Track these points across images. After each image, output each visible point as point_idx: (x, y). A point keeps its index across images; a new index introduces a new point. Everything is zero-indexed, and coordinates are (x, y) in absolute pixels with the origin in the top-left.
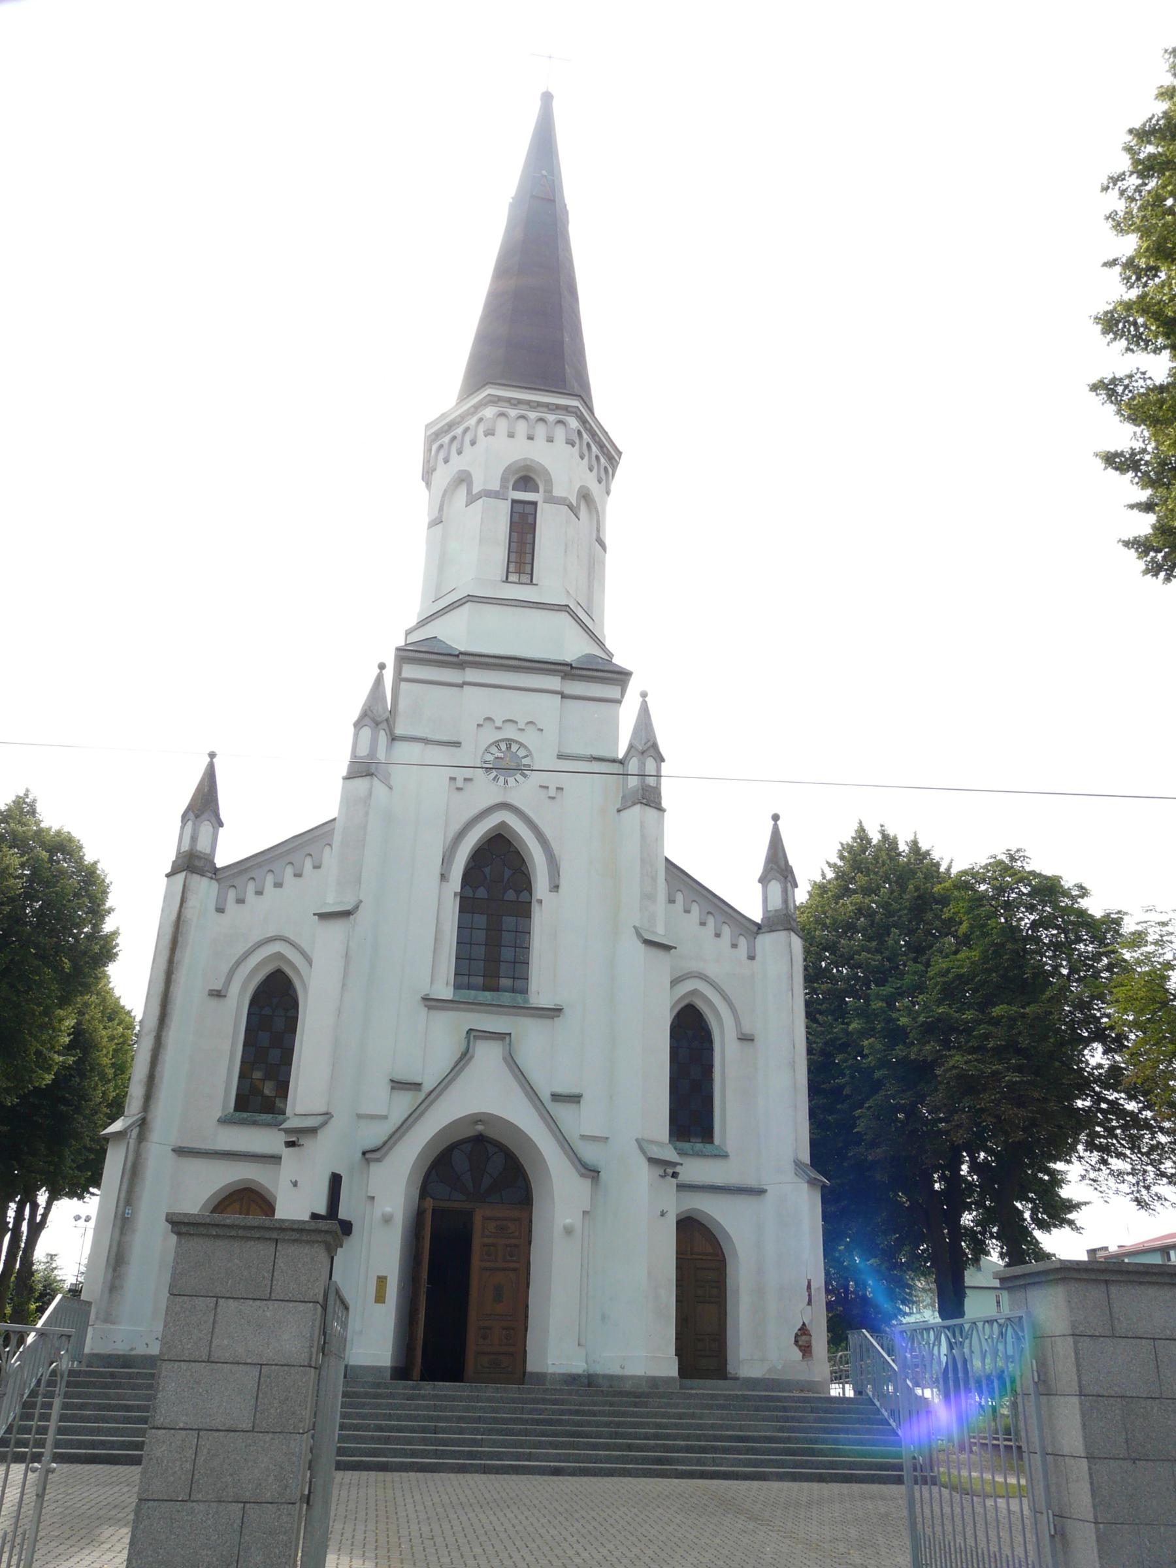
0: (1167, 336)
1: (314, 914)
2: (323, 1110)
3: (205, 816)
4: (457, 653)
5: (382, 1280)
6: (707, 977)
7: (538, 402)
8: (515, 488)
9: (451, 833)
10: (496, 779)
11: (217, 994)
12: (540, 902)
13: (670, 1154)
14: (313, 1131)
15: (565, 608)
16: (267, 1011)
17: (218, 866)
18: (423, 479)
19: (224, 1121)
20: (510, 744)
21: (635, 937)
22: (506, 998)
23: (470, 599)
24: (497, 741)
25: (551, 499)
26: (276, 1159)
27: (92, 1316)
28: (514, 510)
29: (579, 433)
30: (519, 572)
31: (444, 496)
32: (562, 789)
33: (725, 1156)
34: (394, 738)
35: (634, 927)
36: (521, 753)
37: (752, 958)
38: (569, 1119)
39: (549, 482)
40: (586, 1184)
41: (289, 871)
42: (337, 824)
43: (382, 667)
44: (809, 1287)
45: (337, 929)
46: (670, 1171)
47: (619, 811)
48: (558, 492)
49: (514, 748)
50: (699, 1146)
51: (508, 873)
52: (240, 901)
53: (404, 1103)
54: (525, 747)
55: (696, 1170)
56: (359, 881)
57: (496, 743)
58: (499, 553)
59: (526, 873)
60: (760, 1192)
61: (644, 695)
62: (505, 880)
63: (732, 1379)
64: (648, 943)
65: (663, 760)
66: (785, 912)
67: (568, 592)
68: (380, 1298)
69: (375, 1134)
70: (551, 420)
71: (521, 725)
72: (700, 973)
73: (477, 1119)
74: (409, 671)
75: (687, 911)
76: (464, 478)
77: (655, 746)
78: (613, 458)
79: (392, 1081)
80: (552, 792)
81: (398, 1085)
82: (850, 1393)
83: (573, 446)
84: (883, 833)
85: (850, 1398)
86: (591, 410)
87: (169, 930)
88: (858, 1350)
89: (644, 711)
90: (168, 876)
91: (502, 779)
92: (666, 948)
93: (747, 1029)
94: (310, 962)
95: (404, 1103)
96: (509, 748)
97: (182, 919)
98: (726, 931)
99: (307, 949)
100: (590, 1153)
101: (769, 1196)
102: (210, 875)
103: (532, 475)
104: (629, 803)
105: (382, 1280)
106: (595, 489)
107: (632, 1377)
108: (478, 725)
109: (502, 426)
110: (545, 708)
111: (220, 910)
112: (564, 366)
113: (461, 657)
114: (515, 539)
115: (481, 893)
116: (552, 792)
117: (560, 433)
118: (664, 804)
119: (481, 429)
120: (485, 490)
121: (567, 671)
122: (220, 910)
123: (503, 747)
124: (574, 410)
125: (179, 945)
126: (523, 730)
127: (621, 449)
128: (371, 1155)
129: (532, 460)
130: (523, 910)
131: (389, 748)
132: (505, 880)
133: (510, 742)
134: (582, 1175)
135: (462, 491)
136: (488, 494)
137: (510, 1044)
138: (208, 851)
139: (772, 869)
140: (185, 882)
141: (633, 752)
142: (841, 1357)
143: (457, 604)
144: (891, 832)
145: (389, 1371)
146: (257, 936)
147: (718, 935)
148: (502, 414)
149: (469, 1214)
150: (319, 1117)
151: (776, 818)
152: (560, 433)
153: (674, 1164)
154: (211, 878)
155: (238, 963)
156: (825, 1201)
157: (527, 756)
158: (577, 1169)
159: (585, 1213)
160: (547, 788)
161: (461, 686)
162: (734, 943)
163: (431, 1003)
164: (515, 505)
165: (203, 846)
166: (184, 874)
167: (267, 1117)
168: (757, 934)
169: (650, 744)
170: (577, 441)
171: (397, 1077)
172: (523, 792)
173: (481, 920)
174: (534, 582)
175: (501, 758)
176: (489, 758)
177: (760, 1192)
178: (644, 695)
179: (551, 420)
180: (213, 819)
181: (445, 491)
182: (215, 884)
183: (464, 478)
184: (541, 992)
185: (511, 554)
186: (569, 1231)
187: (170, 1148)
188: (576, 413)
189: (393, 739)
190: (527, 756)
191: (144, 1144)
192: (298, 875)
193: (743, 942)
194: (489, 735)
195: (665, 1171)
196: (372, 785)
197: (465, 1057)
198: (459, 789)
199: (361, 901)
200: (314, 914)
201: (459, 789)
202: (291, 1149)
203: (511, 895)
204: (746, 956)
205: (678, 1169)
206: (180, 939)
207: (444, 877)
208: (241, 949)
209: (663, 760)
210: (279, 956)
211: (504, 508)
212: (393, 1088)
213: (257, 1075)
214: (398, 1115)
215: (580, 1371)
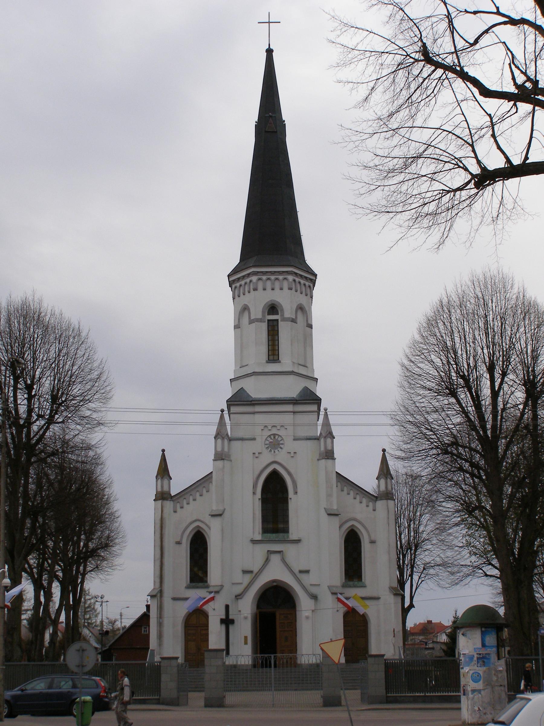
2: (220, 584)
4: (251, 399)
5: (246, 638)
8: (269, 314)
9: (255, 476)
10: (271, 451)
11: (179, 543)
19: (188, 587)
22: (281, 536)
25: (284, 319)
27: (155, 654)
28: (269, 325)
33: (365, 586)
36: (280, 439)
37: (374, 510)
38: (307, 580)
39: (282, 310)
41: (198, 494)
42: (214, 475)
43: (222, 411)
44: (394, 631)
45: (218, 520)
47: (318, 460)
48: (287, 315)
49: (277, 437)
50: (356, 583)
52: (182, 507)
53: (247, 578)
54: (281, 436)
55: (352, 592)
57: (270, 436)
58: (264, 349)
59: (313, 273)
60: (378, 598)
64: (329, 514)
68: (246, 643)
69: (239, 589)
74: (233, 409)
75: (348, 494)
80: (292, 454)
81: (245, 572)
87: (158, 522)
90: (154, 500)
91: (273, 451)
92: (337, 515)
94: (210, 528)
95: (247, 578)
96: (274, 437)
98: (364, 500)
99: (208, 524)
100: (314, 590)
101: (381, 601)
102: (169, 499)
104: (321, 458)
105: (246, 638)
110: (288, 419)
111: (175, 512)
116: (292, 454)
117: (285, 285)
118: (335, 456)
120: (256, 319)
122: (175, 512)
123: (272, 437)
128: (238, 597)
130: (285, 500)
131: (229, 444)
133: (274, 435)
136: (257, 320)
138: (168, 490)
139: (381, 474)
143: (249, 375)
146: (189, 520)
148: (260, 279)
152: (285, 285)
154: (170, 500)
163: (254, 542)
165: (166, 489)
167: (201, 584)
168: (376, 500)
169: (328, 433)
172: (281, 456)
176: (267, 442)
177: (378, 598)
180: (168, 478)
182: (172, 502)
184: (293, 534)
186: (307, 618)
192: (201, 495)
193: (371, 504)
194: (267, 433)
196: (224, 464)
197: (267, 561)
206: (163, 526)
207: (254, 493)
208: (184, 525)
210: (198, 526)
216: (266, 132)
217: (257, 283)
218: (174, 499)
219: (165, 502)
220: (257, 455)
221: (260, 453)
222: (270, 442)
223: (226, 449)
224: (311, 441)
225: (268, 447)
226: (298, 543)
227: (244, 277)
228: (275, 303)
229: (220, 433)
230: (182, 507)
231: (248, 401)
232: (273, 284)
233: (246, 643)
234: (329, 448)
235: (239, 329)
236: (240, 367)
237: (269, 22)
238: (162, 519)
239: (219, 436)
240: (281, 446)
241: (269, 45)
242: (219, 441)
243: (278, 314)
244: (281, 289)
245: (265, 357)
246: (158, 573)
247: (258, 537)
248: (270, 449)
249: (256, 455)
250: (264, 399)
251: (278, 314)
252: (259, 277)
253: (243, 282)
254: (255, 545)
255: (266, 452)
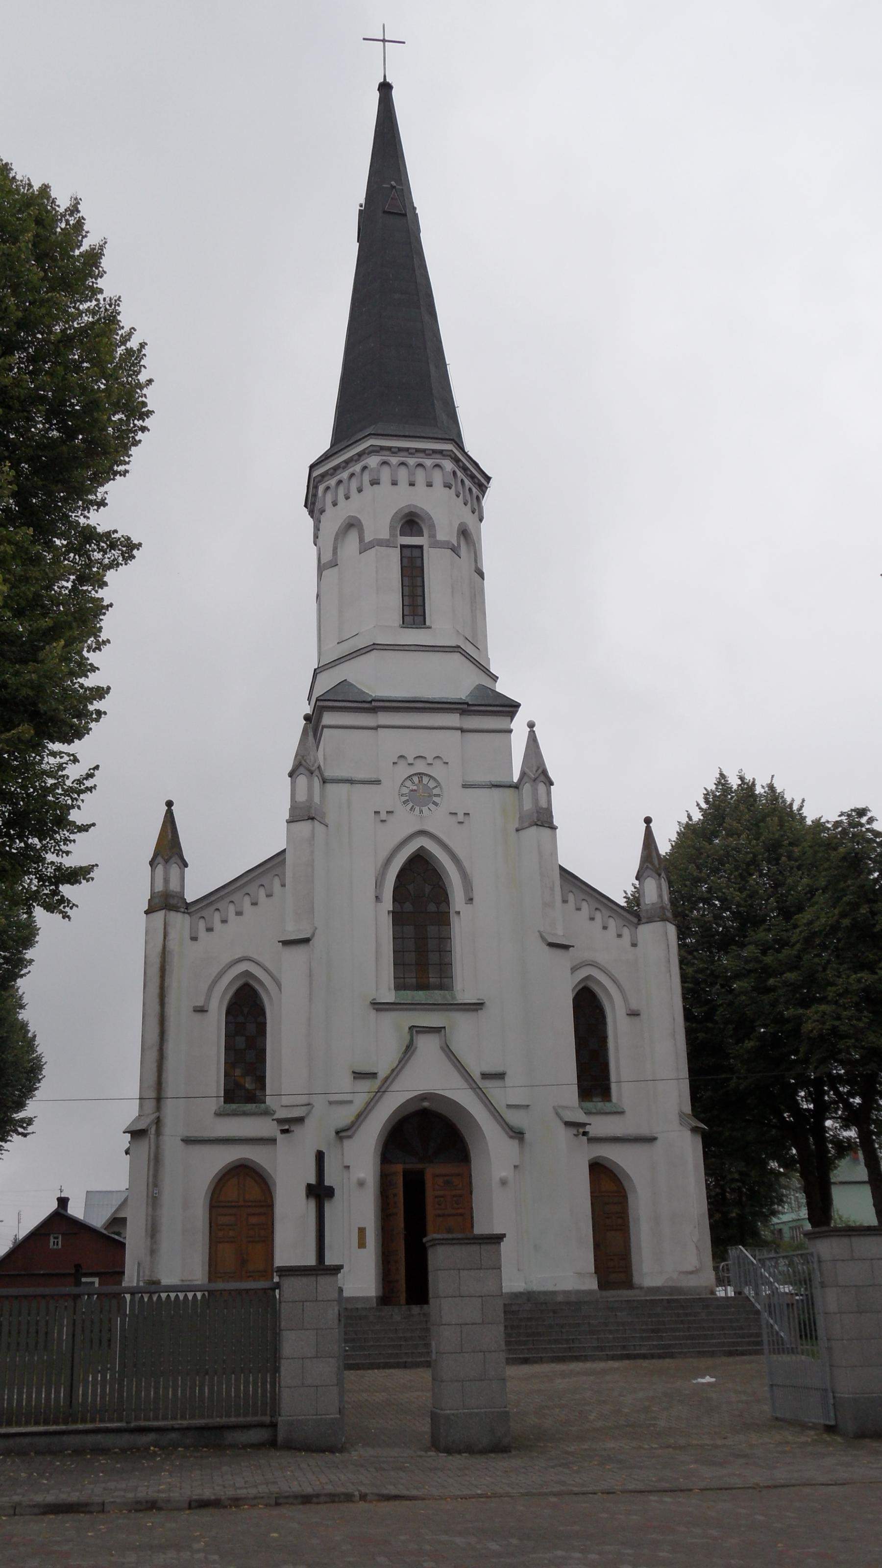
0: (841, 1065)
1: (279, 942)
3: (173, 860)
4: (370, 699)
5: (362, 1231)
6: (597, 963)
7: (416, 449)
11: (201, 1010)
12: (458, 913)
13: (581, 1117)
14: (300, 1120)
15: (457, 649)
16: (241, 1019)
17: (188, 901)
18: (306, 506)
19: (218, 1114)
20: (421, 777)
21: (540, 940)
22: (437, 996)
23: (374, 647)
24: (411, 776)
26: (272, 1141)
29: (454, 473)
30: (414, 614)
31: (336, 539)
32: (468, 814)
34: (324, 781)
35: (539, 931)
36: (432, 784)
37: (634, 945)
39: (432, 527)
40: (515, 1143)
42: (289, 856)
45: (298, 953)
46: (581, 1130)
47: (517, 830)
48: (441, 536)
49: (425, 780)
50: (600, 1105)
51: (428, 888)
55: (600, 1126)
56: (311, 911)
57: (410, 777)
58: (394, 600)
60: (652, 1140)
61: (531, 725)
62: (427, 895)
63: (637, 1288)
64: (551, 945)
65: (552, 784)
66: (661, 905)
67: (458, 631)
68: (362, 1244)
69: (344, 1116)
70: (429, 465)
71: (430, 761)
72: (592, 961)
73: (424, 1097)
76: (352, 525)
77: (545, 773)
78: (483, 484)
79: (354, 1072)
80: (461, 817)
81: (359, 1075)
82: (731, 1293)
83: (450, 488)
84: (742, 778)
85: (731, 1297)
86: (462, 449)
87: (156, 961)
88: (736, 1262)
89: (532, 740)
90: (146, 912)
91: (417, 809)
92: (566, 947)
93: (634, 1006)
96: (420, 781)
97: (167, 949)
98: (612, 923)
100: (515, 1119)
101: (658, 1143)
102: (182, 910)
103: (417, 520)
105: (362, 1231)
106: (469, 520)
107: (565, 1292)
108: (394, 763)
109: (385, 475)
111: (194, 939)
112: (433, 401)
113: (373, 703)
114: (406, 583)
115: (408, 907)
116: (461, 817)
118: (556, 822)
119: (366, 477)
121: (463, 708)
124: (449, 453)
125: (167, 972)
126: (431, 764)
127: (489, 475)
128: (342, 1134)
129: (415, 506)
130: (443, 919)
132: (427, 895)
134: (511, 1137)
135: (353, 538)
136: (380, 543)
137: (445, 1035)
138: (178, 889)
140: (165, 919)
141: (526, 779)
142: (723, 1267)
144: (749, 778)
145: (375, 1300)
146: (227, 958)
147: (605, 928)
148: (385, 463)
149: (421, 1173)
150: (302, 1107)
151: (648, 821)
152: (438, 478)
153: (584, 1125)
154: (184, 912)
155: (215, 982)
156: (705, 1146)
157: (436, 787)
158: (507, 1133)
159: (516, 1167)
160: (456, 814)
161: (376, 728)
162: (619, 933)
163: (379, 1006)
164: (404, 550)
165: (174, 886)
166: (164, 911)
169: (540, 771)
170: (453, 483)
171: (357, 1070)
173: (409, 930)
174: (428, 623)
175: (415, 790)
176: (405, 791)
177: (652, 1140)
178: (531, 725)
179: (429, 465)
180: (179, 861)
181: (337, 534)
183: (352, 525)
185: (405, 598)
186: (504, 1182)
187: (180, 1138)
188: (450, 456)
189: (324, 782)
190: (436, 787)
191: (161, 1137)
192: (254, 904)
193: (626, 932)
194: (404, 771)
195: (578, 1131)
196: (314, 828)
197: (409, 1049)
198: (383, 821)
199: (316, 928)
200: (279, 942)
201: (383, 821)
202: (284, 1135)
203: (432, 907)
204: (630, 944)
205: (588, 1128)
206: (167, 967)
208: (214, 972)
209: (552, 784)
210: (247, 973)
211: (395, 554)
212: (354, 1078)
213: (238, 1072)
214: (360, 1101)
215: (521, 1290)
216: (385, 212)
217: (379, 471)
218: (194, 909)
219: (172, 915)
220: (383, 816)
221: (392, 812)
222: (412, 791)
223: (317, 799)
224: (501, 789)
225: (407, 801)
226: (476, 1010)
227: (347, 462)
228: (418, 512)
229: (303, 763)
230: (210, 930)
231: (364, 702)
232: (411, 474)
233: (362, 1244)
234: (543, 804)
235: (336, 569)
236: (338, 643)
237: (384, 41)
238: (164, 953)
239: (301, 770)
240: (435, 799)
241: (385, 76)
242: (302, 780)
243: (423, 536)
244: (429, 485)
245: (396, 617)
246: (152, 1078)
247: (388, 996)
248: (411, 805)
249: (382, 817)
250: (400, 699)
251: (423, 536)
252: (384, 458)
253: (345, 475)
254: (379, 1013)
255: (402, 811)
